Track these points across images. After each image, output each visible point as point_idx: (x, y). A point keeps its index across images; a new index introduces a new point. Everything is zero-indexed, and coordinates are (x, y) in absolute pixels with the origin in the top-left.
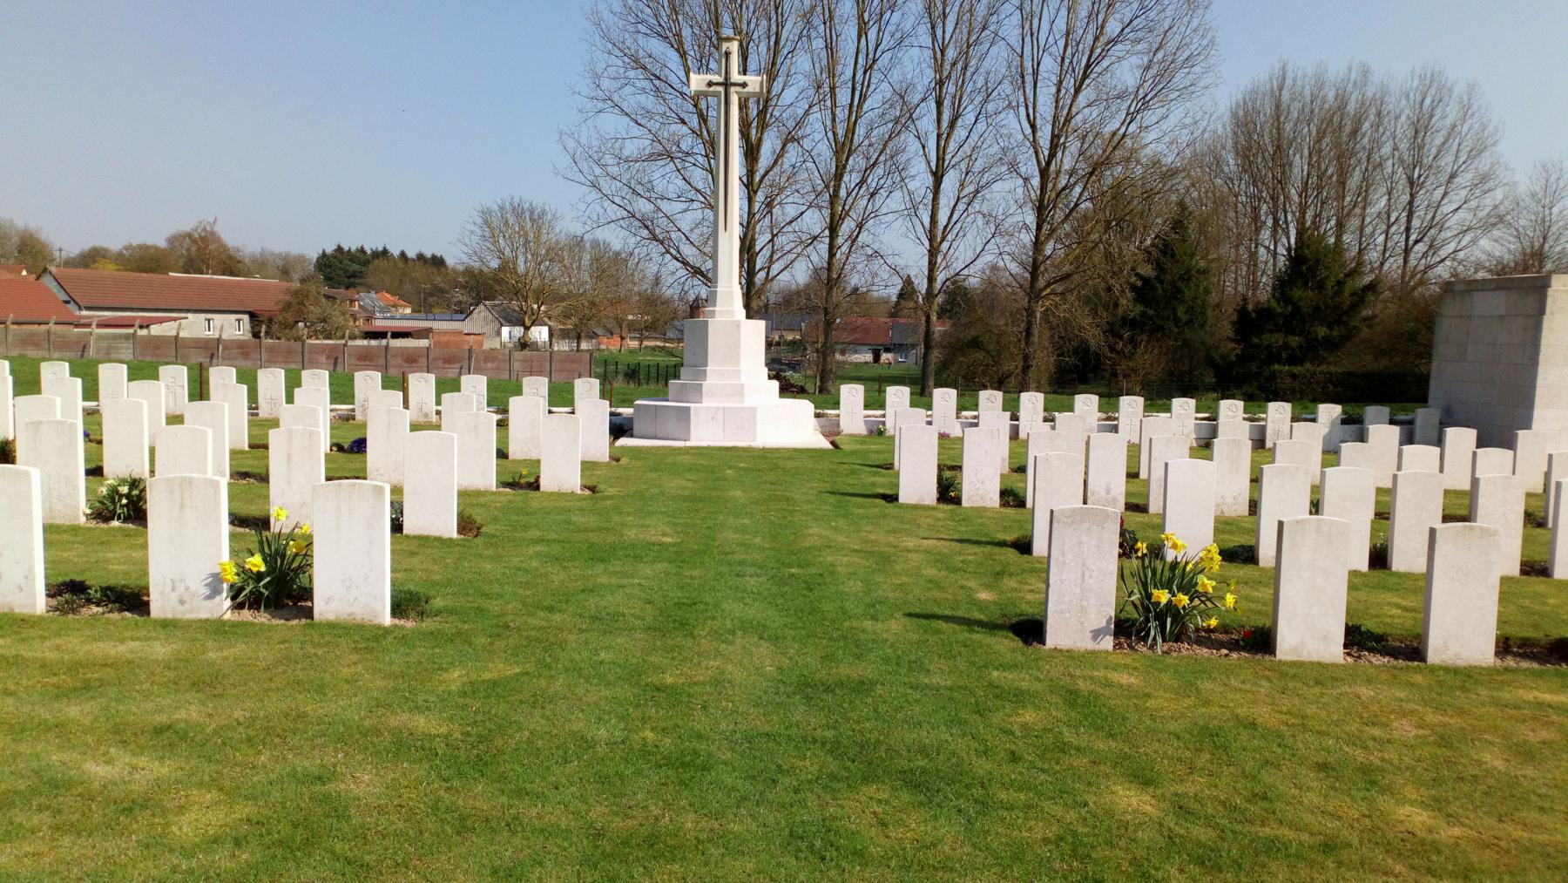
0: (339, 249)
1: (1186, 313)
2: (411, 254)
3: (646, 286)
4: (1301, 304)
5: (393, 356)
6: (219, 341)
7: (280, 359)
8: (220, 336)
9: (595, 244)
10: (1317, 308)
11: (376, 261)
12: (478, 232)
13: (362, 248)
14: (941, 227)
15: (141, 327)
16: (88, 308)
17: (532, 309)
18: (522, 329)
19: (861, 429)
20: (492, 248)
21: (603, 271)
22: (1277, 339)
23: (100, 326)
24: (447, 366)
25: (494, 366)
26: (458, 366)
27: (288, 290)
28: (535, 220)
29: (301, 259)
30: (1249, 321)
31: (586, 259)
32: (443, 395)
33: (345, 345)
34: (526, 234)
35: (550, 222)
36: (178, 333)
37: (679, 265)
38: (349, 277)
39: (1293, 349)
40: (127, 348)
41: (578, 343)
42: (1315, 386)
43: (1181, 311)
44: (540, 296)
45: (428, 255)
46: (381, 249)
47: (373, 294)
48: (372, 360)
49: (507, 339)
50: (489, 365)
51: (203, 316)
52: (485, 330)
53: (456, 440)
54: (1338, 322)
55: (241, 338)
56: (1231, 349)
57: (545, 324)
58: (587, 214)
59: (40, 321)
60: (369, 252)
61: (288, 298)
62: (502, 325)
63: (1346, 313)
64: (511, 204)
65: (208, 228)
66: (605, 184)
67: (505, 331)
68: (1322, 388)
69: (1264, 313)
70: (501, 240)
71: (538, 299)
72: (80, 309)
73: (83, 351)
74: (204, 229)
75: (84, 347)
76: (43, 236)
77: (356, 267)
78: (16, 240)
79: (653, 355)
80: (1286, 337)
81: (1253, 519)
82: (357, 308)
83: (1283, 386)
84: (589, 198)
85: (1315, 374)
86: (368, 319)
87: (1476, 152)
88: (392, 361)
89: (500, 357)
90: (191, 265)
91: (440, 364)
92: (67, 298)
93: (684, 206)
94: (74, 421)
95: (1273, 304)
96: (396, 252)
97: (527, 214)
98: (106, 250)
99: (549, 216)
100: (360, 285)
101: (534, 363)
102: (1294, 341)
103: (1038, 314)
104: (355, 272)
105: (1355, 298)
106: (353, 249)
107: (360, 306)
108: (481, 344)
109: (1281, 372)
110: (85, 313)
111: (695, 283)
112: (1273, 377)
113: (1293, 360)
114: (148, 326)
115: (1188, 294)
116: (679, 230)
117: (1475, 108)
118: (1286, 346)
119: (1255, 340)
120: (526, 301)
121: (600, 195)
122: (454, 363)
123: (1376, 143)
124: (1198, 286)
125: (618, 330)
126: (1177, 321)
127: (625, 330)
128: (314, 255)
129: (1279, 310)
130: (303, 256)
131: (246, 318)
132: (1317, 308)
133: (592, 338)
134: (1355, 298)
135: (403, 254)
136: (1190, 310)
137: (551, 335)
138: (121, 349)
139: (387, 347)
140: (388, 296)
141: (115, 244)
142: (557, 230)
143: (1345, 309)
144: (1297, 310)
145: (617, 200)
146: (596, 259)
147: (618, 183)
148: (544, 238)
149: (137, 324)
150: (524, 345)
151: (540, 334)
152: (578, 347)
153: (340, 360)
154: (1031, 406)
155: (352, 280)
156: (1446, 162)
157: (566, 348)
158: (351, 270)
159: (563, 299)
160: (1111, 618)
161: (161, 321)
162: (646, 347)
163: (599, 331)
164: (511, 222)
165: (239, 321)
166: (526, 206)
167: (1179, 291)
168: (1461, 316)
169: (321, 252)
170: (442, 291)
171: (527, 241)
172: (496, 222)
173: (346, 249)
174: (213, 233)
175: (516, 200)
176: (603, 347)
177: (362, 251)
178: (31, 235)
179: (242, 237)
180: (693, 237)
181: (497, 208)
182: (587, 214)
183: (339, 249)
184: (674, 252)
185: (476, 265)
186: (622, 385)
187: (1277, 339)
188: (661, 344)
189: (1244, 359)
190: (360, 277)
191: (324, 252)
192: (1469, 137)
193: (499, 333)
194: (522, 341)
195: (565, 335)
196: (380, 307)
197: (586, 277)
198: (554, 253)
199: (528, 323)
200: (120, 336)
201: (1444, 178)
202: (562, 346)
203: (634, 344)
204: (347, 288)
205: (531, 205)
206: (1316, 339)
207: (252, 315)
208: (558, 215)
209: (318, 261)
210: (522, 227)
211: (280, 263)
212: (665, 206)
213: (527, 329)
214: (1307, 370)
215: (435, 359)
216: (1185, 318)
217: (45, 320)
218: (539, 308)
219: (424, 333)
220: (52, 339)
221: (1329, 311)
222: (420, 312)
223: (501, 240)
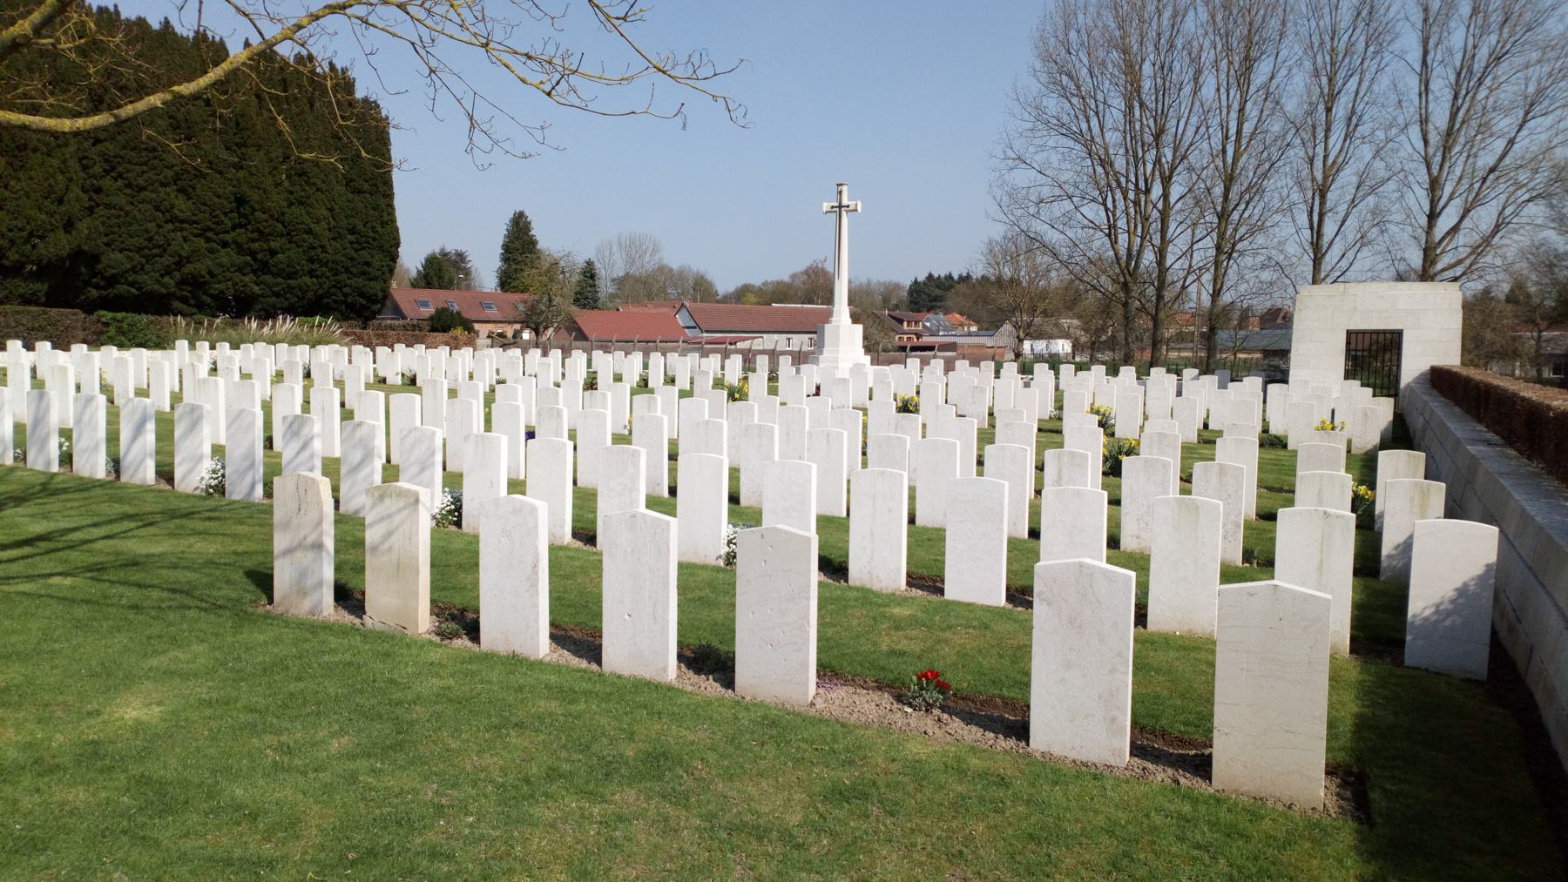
0: (930, 276)
14: (1136, 248)
15: (731, 344)
16: (707, 332)
32: (391, 396)
38: (931, 301)
46: (964, 275)
47: (941, 316)
53: (1090, 458)
59: (648, 339)
60: (956, 277)
76: (709, 277)
77: (938, 292)
78: (691, 282)
81: (1033, 542)
94: (376, 423)
98: (753, 286)
104: (937, 296)
106: (943, 275)
110: (705, 335)
114: (735, 343)
128: (907, 282)
140: (958, 316)
141: (757, 281)
160: (92, 578)
173: (936, 275)
177: (950, 277)
178: (702, 277)
183: (930, 276)
190: (940, 301)
217: (654, 339)
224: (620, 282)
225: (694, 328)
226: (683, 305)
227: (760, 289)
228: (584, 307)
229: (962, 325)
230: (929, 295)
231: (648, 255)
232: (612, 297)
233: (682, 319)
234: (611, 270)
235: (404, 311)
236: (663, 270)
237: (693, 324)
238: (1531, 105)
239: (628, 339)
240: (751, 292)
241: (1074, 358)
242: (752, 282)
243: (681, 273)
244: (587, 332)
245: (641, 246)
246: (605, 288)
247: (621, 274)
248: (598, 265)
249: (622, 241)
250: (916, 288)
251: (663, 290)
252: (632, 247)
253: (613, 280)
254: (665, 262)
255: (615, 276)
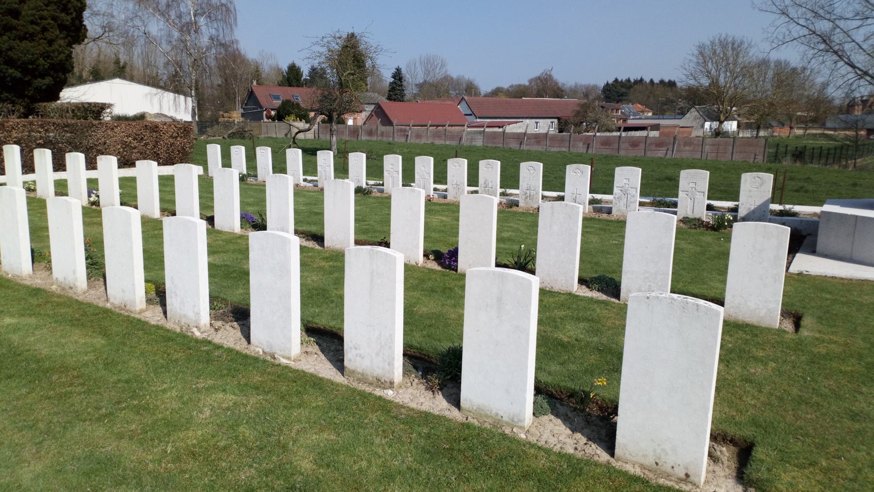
0: (616, 80)
2: (656, 81)
3: (814, 92)
5: (623, 142)
6: (525, 134)
7: (557, 145)
8: (526, 131)
9: (778, 63)
11: (636, 86)
12: (695, 60)
13: (629, 79)
16: (480, 118)
17: (726, 110)
18: (718, 123)
20: (703, 70)
21: (782, 82)
23: (488, 127)
24: (658, 149)
25: (691, 148)
26: (665, 148)
27: (579, 104)
28: (735, 49)
29: (595, 87)
31: (770, 74)
33: (595, 136)
34: (727, 59)
35: (746, 49)
36: (526, 131)
37: (850, 69)
38: (619, 96)
40: (480, 139)
41: (758, 132)
44: (733, 101)
45: (667, 80)
46: (639, 79)
47: (630, 105)
48: (610, 145)
49: (708, 130)
50: (687, 148)
51: (534, 121)
52: (694, 124)
55: (538, 132)
57: (735, 120)
58: (775, 35)
59: (438, 124)
60: (632, 81)
61: (578, 109)
62: (705, 121)
64: (719, 39)
65: (548, 73)
66: (792, 12)
67: (707, 125)
70: (710, 65)
71: (731, 102)
72: (476, 118)
73: (460, 141)
74: (546, 73)
75: (461, 138)
76: (475, 83)
77: (624, 90)
78: (464, 86)
79: (814, 140)
82: (620, 114)
84: (778, 23)
86: (625, 120)
88: (623, 146)
89: (696, 142)
90: (539, 94)
91: (654, 147)
92: (471, 113)
93: (859, 23)
96: (647, 80)
97: (730, 45)
98: (503, 88)
99: (746, 45)
100: (625, 100)
101: (721, 147)
104: (623, 93)
106: (624, 80)
107: (622, 112)
108: (690, 133)
110: (478, 120)
111: (862, 84)
114: (502, 127)
116: (854, 41)
120: (723, 104)
121: (787, 19)
122: (662, 147)
125: (788, 122)
127: (794, 122)
128: (601, 84)
130: (596, 86)
131: (556, 121)
133: (767, 128)
135: (652, 81)
137: (739, 126)
138: (477, 139)
139: (620, 137)
140: (639, 106)
141: (506, 85)
142: (751, 54)
145: (802, 22)
146: (777, 74)
147: (804, 9)
148: (740, 60)
149: (485, 126)
150: (718, 133)
151: (731, 126)
152: (757, 134)
153: (591, 145)
155: (621, 97)
157: (749, 135)
158: (621, 92)
159: (749, 102)
161: (510, 123)
162: (809, 134)
163: (774, 123)
164: (718, 52)
165: (552, 122)
166: (730, 40)
169: (606, 83)
170: (672, 102)
171: (728, 64)
172: (707, 52)
173: (620, 80)
174: (550, 76)
175: (723, 36)
176: (775, 134)
178: (471, 83)
179: (565, 77)
180: (865, 46)
181: (709, 43)
182: (775, 35)
183: (616, 80)
184: (846, 60)
185: (692, 82)
186: (790, 164)
188: (819, 131)
190: (626, 96)
191: (607, 83)
193: (703, 126)
194: (717, 131)
195: (748, 126)
196: (634, 113)
197: (768, 86)
198: (747, 71)
199: (722, 118)
200: (477, 132)
202: (747, 134)
203: (800, 132)
204: (617, 102)
205: (733, 38)
207: (559, 119)
208: (753, 43)
209: (604, 88)
210: (725, 54)
211: (584, 90)
212: (841, 24)
213: (721, 122)
215: (650, 144)
217: (444, 124)
218: (731, 108)
219: (656, 127)
220: (447, 133)
222: (657, 115)
223: (710, 65)
224: (420, 86)
225: (471, 115)
226: (463, 98)
227: (508, 90)
228: (395, 100)
229: (643, 112)
230: (618, 92)
231: (438, 69)
232: (415, 96)
233: (463, 108)
234: (413, 79)
235: (262, 104)
236: (447, 78)
237: (470, 112)
238: (33, 426)
239: (424, 123)
240: (501, 92)
241: (738, 135)
242: (502, 86)
243: (458, 80)
244: (392, 118)
245: (434, 62)
246: (410, 90)
247: (421, 81)
248: (404, 71)
249: (422, 59)
250: (608, 88)
251: (447, 91)
252: (429, 63)
253: (416, 85)
254: (448, 73)
255: (418, 82)
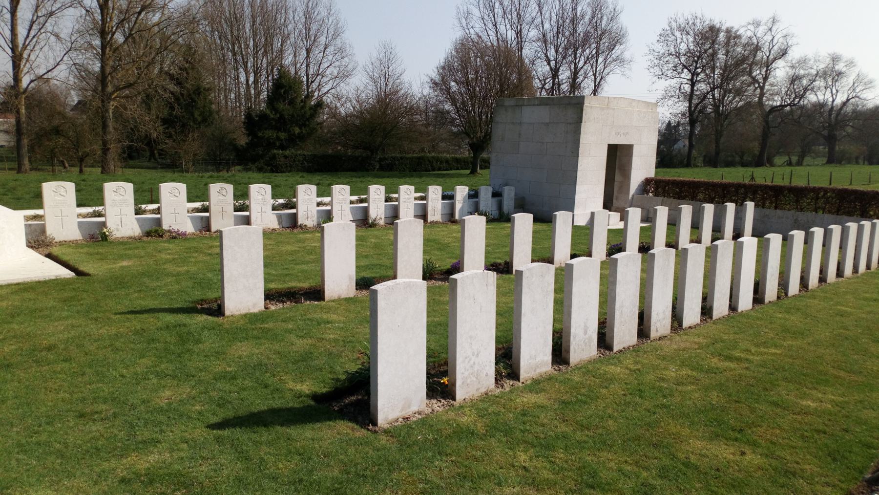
1: (200, 115)
4: (284, 113)
10: (293, 116)
19: (74, 234)
22: (270, 134)
30: (253, 122)
39: (282, 140)
42: (297, 163)
43: (197, 114)
54: (304, 125)
56: (243, 140)
63: (308, 119)
68: (301, 164)
69: (263, 116)
80: (277, 132)
83: (280, 163)
85: (296, 155)
87: (336, 35)
95: (268, 112)
102: (283, 135)
103: (111, 112)
105: (312, 111)
109: (278, 154)
112: (274, 157)
113: (283, 147)
115: (200, 103)
117: (333, 11)
118: (278, 138)
119: (260, 134)
123: (285, 25)
124: (206, 99)
126: (195, 120)
129: (272, 116)
132: (293, 116)
134: (312, 111)
136: (202, 114)
143: (307, 117)
144: (282, 117)
154: (260, 197)
156: (322, 40)
167: (193, 101)
168: (513, 123)
187: (270, 134)
189: (251, 145)
192: (332, 26)
201: (322, 48)
206: (294, 134)
214: (292, 153)
216: (199, 119)
221: (299, 118)
